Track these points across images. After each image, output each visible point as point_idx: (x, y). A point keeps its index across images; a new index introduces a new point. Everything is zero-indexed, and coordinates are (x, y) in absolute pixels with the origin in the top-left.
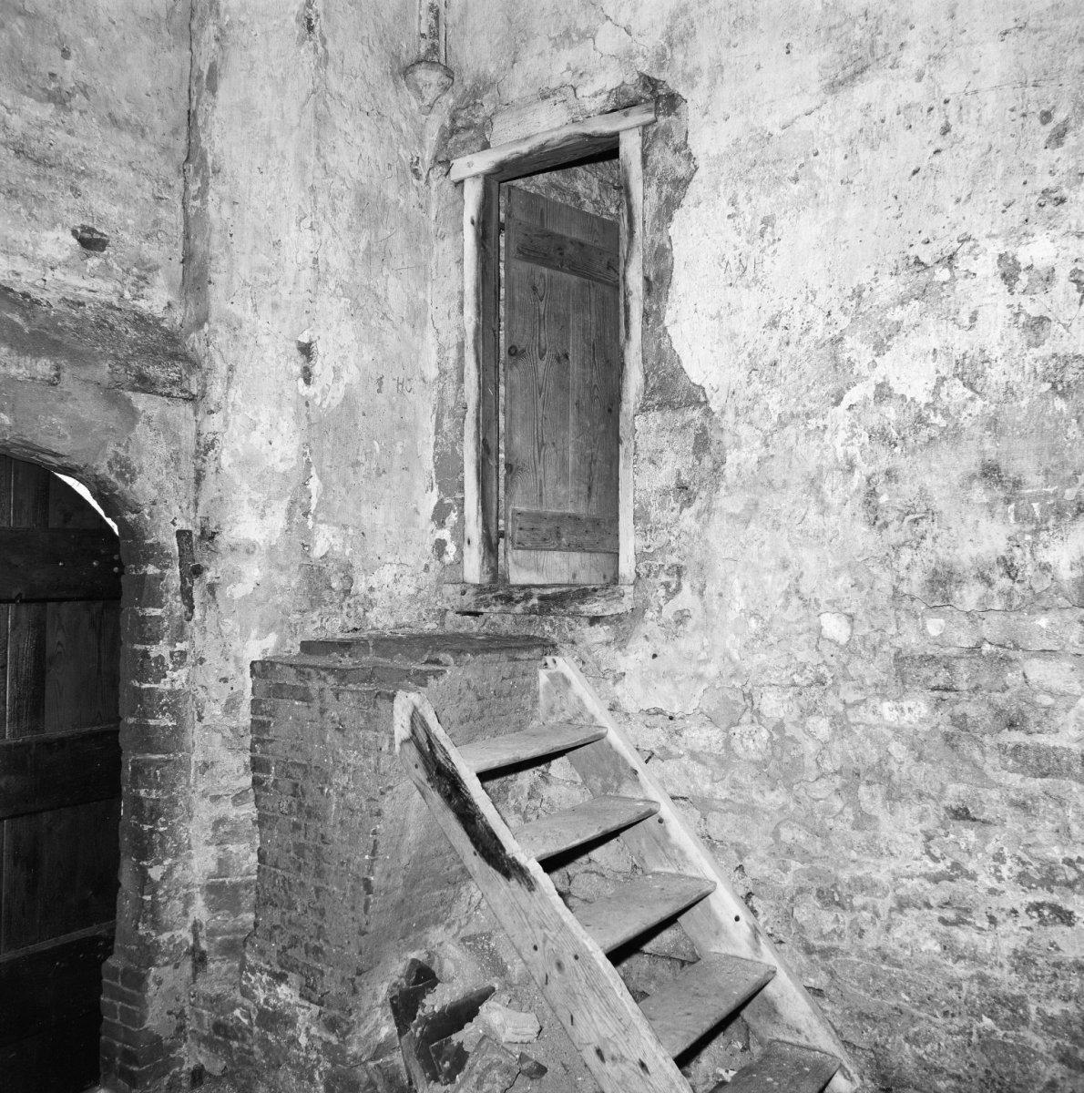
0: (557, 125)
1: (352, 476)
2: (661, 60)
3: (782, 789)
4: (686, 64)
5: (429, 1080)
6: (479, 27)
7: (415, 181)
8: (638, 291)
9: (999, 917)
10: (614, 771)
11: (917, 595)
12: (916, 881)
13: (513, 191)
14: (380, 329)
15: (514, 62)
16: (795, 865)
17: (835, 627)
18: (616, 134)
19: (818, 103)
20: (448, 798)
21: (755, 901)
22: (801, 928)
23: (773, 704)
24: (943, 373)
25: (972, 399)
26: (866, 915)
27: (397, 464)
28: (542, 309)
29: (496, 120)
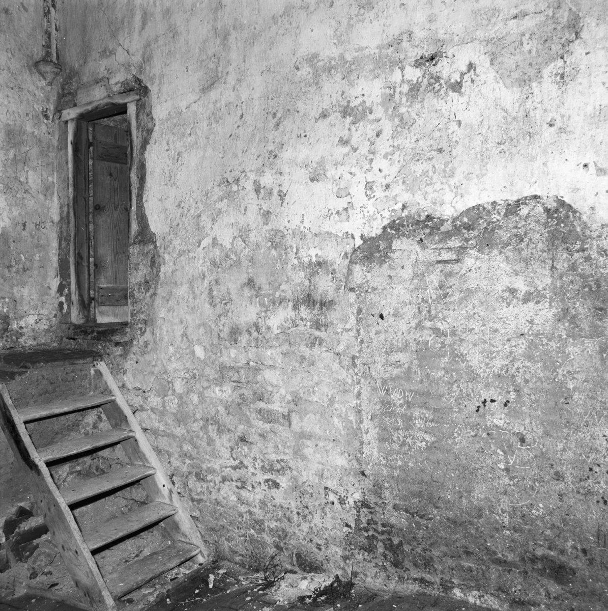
0: (102, 97)
1: (7, 272)
2: (141, 69)
3: (182, 426)
4: (150, 72)
5: (17, 561)
6: (72, 43)
7: (45, 121)
8: (134, 183)
9: (255, 485)
10: (118, 418)
11: (226, 338)
12: (228, 469)
13: (96, 126)
14: (23, 198)
15: (85, 63)
16: (188, 461)
17: (199, 352)
18: (126, 104)
19: (198, 97)
20: (11, 433)
21: (174, 478)
22: (190, 490)
23: (179, 387)
24: (235, 234)
25: (245, 248)
26: (212, 484)
27: (36, 265)
28: (116, 185)
29: (79, 92)
